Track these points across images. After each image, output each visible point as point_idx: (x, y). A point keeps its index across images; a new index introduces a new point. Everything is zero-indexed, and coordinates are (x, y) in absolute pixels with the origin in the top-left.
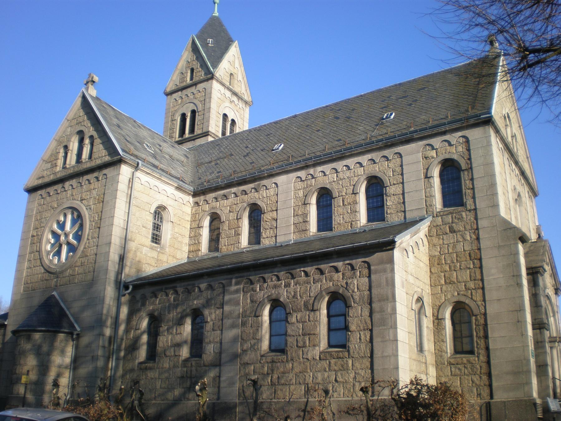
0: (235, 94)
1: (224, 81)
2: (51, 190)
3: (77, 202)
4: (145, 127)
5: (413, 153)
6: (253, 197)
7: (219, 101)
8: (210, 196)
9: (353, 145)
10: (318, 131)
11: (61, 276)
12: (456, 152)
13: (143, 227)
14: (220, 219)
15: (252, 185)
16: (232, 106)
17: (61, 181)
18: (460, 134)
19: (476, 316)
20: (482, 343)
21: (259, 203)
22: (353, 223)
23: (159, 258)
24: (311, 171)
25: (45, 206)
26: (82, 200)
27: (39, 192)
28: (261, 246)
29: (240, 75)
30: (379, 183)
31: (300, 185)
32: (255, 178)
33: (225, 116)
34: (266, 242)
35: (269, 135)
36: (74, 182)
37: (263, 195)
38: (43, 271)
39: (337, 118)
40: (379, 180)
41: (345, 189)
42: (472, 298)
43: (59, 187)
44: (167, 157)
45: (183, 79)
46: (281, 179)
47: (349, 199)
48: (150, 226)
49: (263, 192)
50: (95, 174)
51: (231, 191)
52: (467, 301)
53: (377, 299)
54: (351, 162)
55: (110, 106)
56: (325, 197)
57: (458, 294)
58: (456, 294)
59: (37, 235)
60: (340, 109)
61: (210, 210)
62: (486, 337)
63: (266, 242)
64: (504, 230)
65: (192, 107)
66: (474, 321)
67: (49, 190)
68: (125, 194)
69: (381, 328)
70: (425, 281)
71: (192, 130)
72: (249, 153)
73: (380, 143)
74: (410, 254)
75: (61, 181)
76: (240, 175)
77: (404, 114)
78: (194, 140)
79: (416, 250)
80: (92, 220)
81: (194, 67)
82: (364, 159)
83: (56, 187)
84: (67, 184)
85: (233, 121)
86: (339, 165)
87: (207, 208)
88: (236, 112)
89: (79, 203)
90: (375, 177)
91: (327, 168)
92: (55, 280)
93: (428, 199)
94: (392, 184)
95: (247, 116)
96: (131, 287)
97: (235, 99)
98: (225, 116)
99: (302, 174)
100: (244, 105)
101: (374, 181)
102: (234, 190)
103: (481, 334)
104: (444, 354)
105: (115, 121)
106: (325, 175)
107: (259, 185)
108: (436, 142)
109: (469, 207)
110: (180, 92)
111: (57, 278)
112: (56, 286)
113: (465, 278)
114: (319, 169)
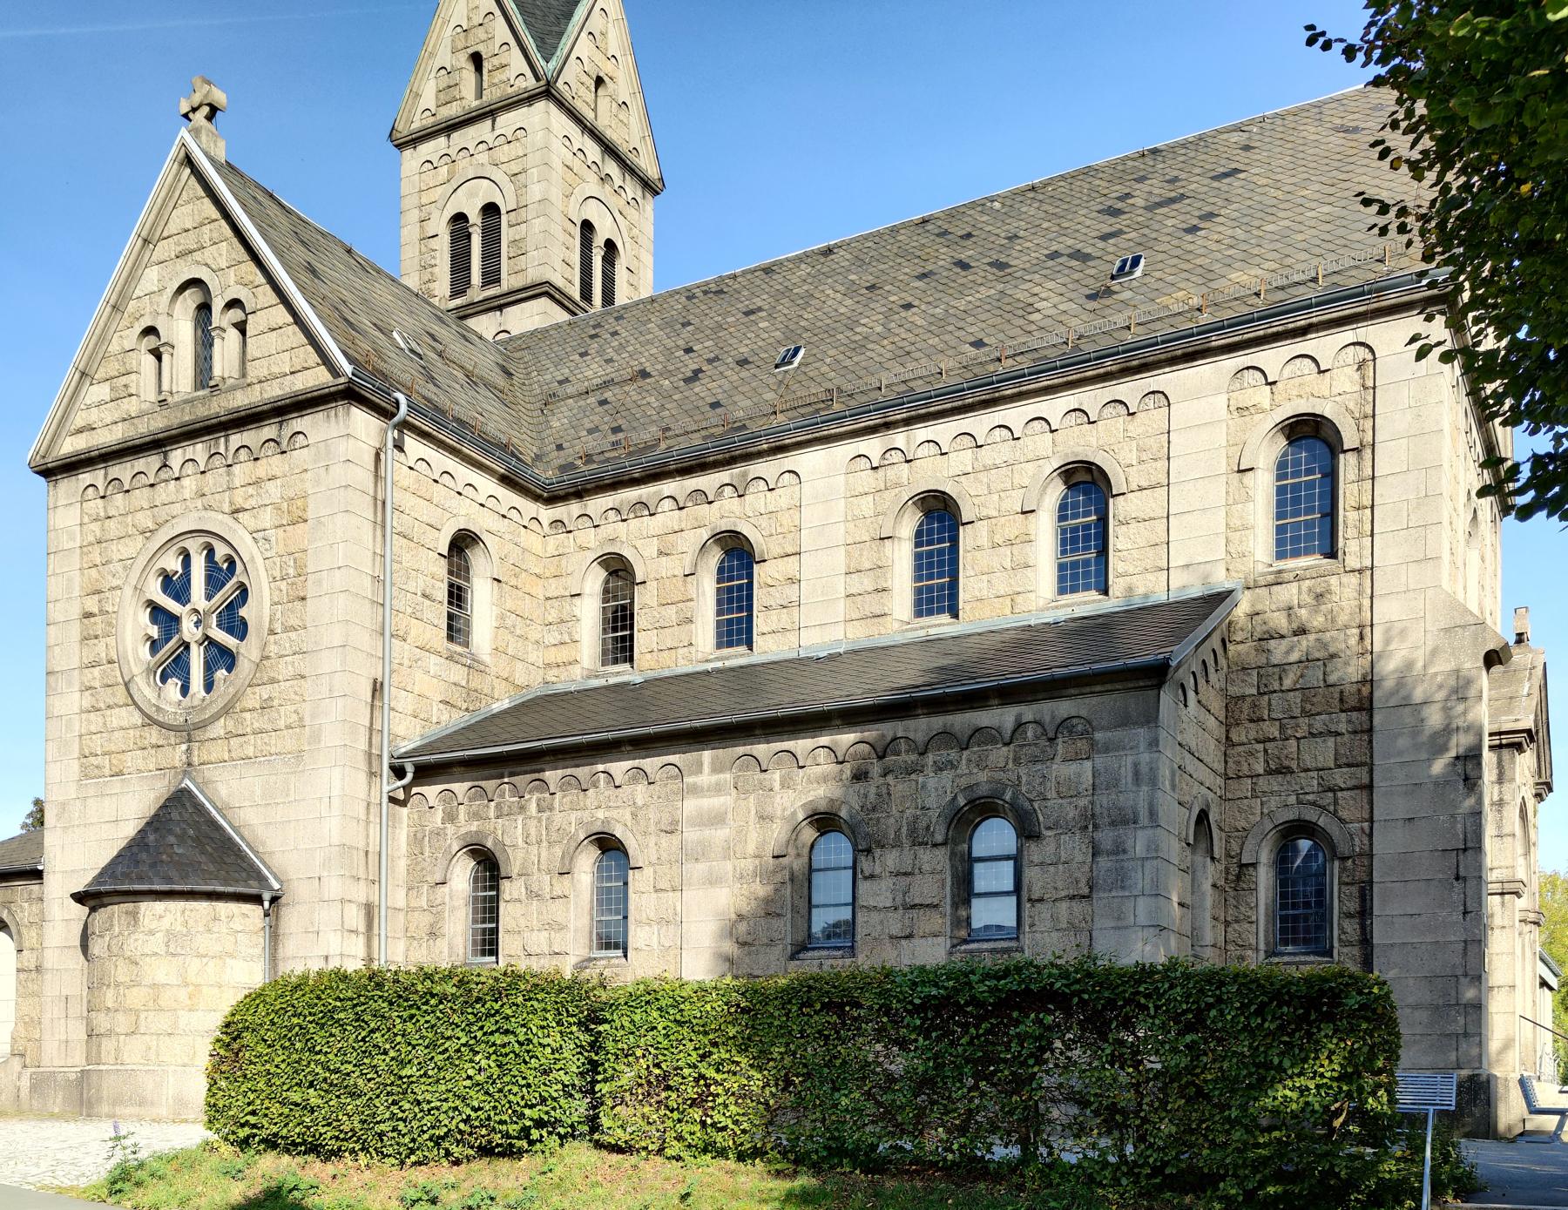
0: (609, 150)
1: (579, 105)
2: (123, 470)
3: (220, 516)
4: (379, 271)
5: (1199, 387)
6: (728, 513)
7: (569, 176)
8: (597, 504)
9: (1025, 363)
10: (908, 306)
11: (198, 735)
12: (1332, 397)
13: (424, 595)
14: (633, 574)
15: (724, 476)
16: (605, 192)
17: (158, 444)
18: (1347, 335)
19: (1344, 859)
20: (1352, 927)
21: (746, 529)
22: (1019, 599)
23: (473, 685)
24: (899, 438)
25: (111, 524)
26: (237, 511)
27: (86, 478)
28: (756, 657)
29: (624, 83)
30: (1093, 482)
31: (867, 480)
32: (730, 452)
33: (587, 227)
34: (769, 645)
35: (752, 312)
36: (198, 450)
37: (758, 502)
38: (137, 719)
39: (964, 266)
40: (1096, 473)
41: (996, 497)
42: (1335, 813)
43: (149, 463)
44: (460, 375)
45: (448, 92)
46: (809, 461)
47: (1012, 527)
48: (442, 593)
49: (757, 499)
50: (266, 429)
51: (660, 492)
52: (1322, 822)
53: (1107, 820)
54: (1015, 415)
55: (271, 196)
56: (940, 515)
57: (1299, 802)
58: (1292, 799)
59: (103, 612)
60: (969, 235)
61: (602, 545)
62: (1364, 913)
63: (769, 645)
64: (1446, 630)
65: (484, 193)
66: (1336, 871)
67: (116, 470)
68: (369, 500)
69: (1114, 894)
70: (1216, 766)
71: (491, 277)
72: (700, 370)
73: (1108, 361)
74: (1191, 694)
75: (158, 444)
76: (683, 443)
77: (1175, 261)
78: (500, 308)
79: (1202, 682)
80: (277, 574)
81: (481, 48)
82: (1055, 407)
83: (140, 464)
84: (177, 456)
85: (610, 245)
86: (978, 423)
87: (589, 537)
88: (617, 215)
89: (228, 520)
90: (1089, 467)
91: (943, 431)
92: (184, 747)
93: (1235, 536)
94: (1135, 487)
95: (649, 228)
96: (410, 769)
97: (612, 168)
98: (587, 227)
99: (872, 446)
100: (639, 193)
101: (1082, 477)
102: (669, 487)
103: (1353, 906)
104: (1249, 952)
105: (300, 254)
106: (940, 454)
107: (745, 474)
108: (1272, 358)
109: (1352, 562)
110: (442, 140)
111: (190, 741)
112: (189, 764)
113: (1321, 758)
114: (922, 432)
